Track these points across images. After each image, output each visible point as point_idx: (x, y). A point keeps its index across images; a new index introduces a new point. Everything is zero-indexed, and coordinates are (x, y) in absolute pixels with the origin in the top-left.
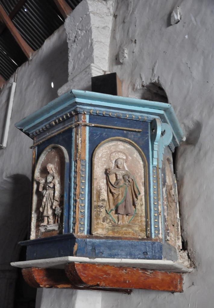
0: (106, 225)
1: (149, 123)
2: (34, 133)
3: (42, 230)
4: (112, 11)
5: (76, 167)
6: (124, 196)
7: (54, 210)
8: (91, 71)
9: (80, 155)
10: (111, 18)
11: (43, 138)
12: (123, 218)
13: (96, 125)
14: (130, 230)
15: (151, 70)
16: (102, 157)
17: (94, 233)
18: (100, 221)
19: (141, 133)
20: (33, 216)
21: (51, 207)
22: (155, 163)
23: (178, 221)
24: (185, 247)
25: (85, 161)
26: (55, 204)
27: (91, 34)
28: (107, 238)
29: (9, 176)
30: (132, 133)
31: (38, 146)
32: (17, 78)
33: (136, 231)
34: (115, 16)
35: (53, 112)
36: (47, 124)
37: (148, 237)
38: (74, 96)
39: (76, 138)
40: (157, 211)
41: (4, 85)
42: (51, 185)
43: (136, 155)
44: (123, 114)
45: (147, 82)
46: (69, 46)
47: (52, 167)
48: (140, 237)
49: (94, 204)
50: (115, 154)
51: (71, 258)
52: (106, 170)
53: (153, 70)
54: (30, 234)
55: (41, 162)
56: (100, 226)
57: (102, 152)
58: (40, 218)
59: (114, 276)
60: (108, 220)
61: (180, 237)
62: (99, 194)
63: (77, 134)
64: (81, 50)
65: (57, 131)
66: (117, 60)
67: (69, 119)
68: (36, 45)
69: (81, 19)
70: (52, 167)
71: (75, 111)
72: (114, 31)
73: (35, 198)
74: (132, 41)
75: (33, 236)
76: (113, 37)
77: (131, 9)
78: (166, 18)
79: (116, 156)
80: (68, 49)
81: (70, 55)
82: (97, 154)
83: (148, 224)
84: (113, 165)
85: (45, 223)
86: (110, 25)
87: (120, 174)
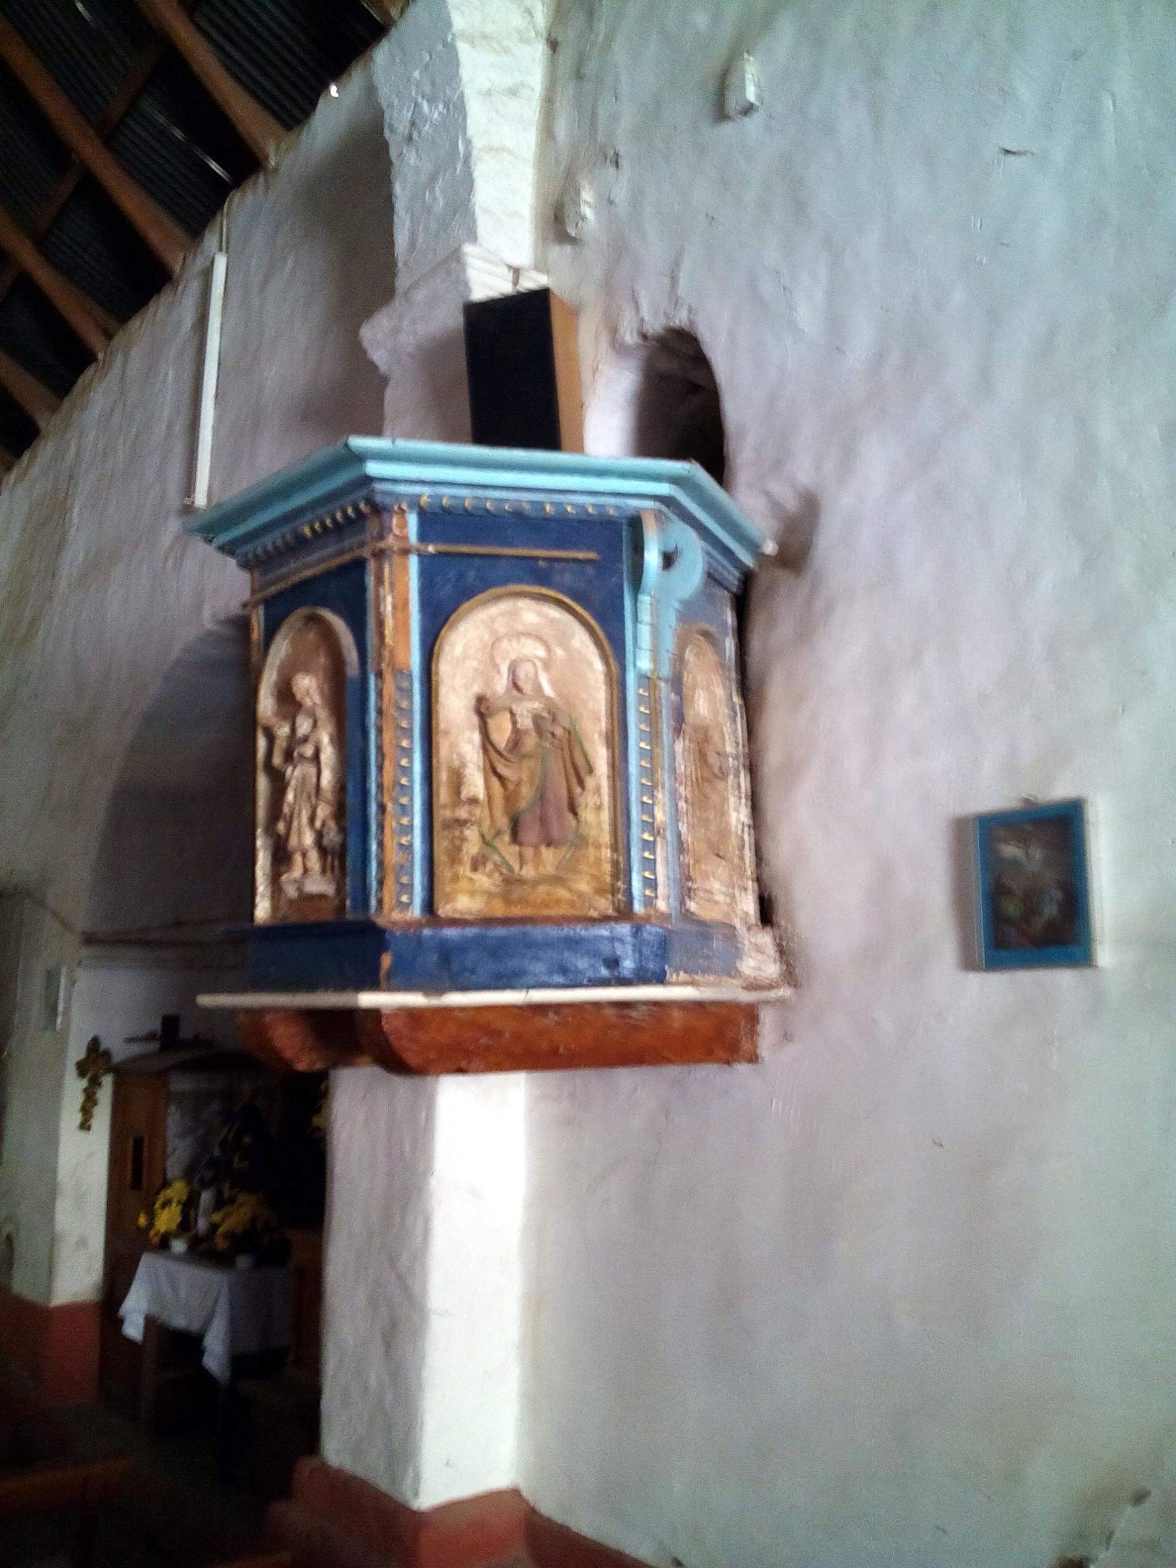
0: (483, 880)
1: (625, 527)
2: (250, 556)
3: (291, 892)
4: (541, 18)
5: (380, 694)
6: (541, 782)
7: (319, 836)
8: (464, 271)
9: (392, 653)
10: (538, 50)
11: (282, 578)
12: (537, 854)
13: (443, 548)
14: (562, 893)
15: (667, 280)
16: (465, 657)
17: (444, 910)
18: (465, 870)
19: (591, 563)
20: (259, 843)
21: (312, 820)
22: (644, 663)
23: (743, 831)
24: (767, 913)
25: (410, 676)
26: (323, 811)
27: (465, 117)
28: (487, 921)
29: (222, 617)
30: (563, 564)
31: (268, 603)
32: (228, 230)
33: (580, 895)
34: (553, 45)
35: (300, 499)
36: (286, 529)
37: (617, 910)
38: (360, 458)
39: (377, 597)
40: (650, 826)
41: (184, 259)
42: (308, 751)
43: (581, 640)
44: (532, 502)
45: (655, 325)
46: (393, 154)
47: (308, 686)
48: (594, 914)
49: (443, 814)
50: (510, 649)
51: (367, 999)
52: (480, 700)
53: (674, 280)
54: (253, 906)
55: (277, 663)
56: (463, 884)
57: (467, 637)
58: (281, 856)
59: (517, 1037)
60: (490, 866)
61: (750, 885)
62: (457, 780)
63: (380, 581)
64: (433, 179)
65: (323, 560)
66: (557, 223)
67: (356, 522)
68: (294, 110)
69: (428, 58)
70: (308, 686)
71: (370, 501)
72: (549, 102)
73: (263, 783)
74: (605, 157)
75: (262, 910)
76: (547, 130)
77: (602, 27)
78: (711, 86)
79: (511, 649)
80: (390, 163)
81: (398, 188)
82: (447, 648)
83: (622, 871)
84: (501, 684)
85: (297, 872)
86: (536, 79)
87: (526, 710)
